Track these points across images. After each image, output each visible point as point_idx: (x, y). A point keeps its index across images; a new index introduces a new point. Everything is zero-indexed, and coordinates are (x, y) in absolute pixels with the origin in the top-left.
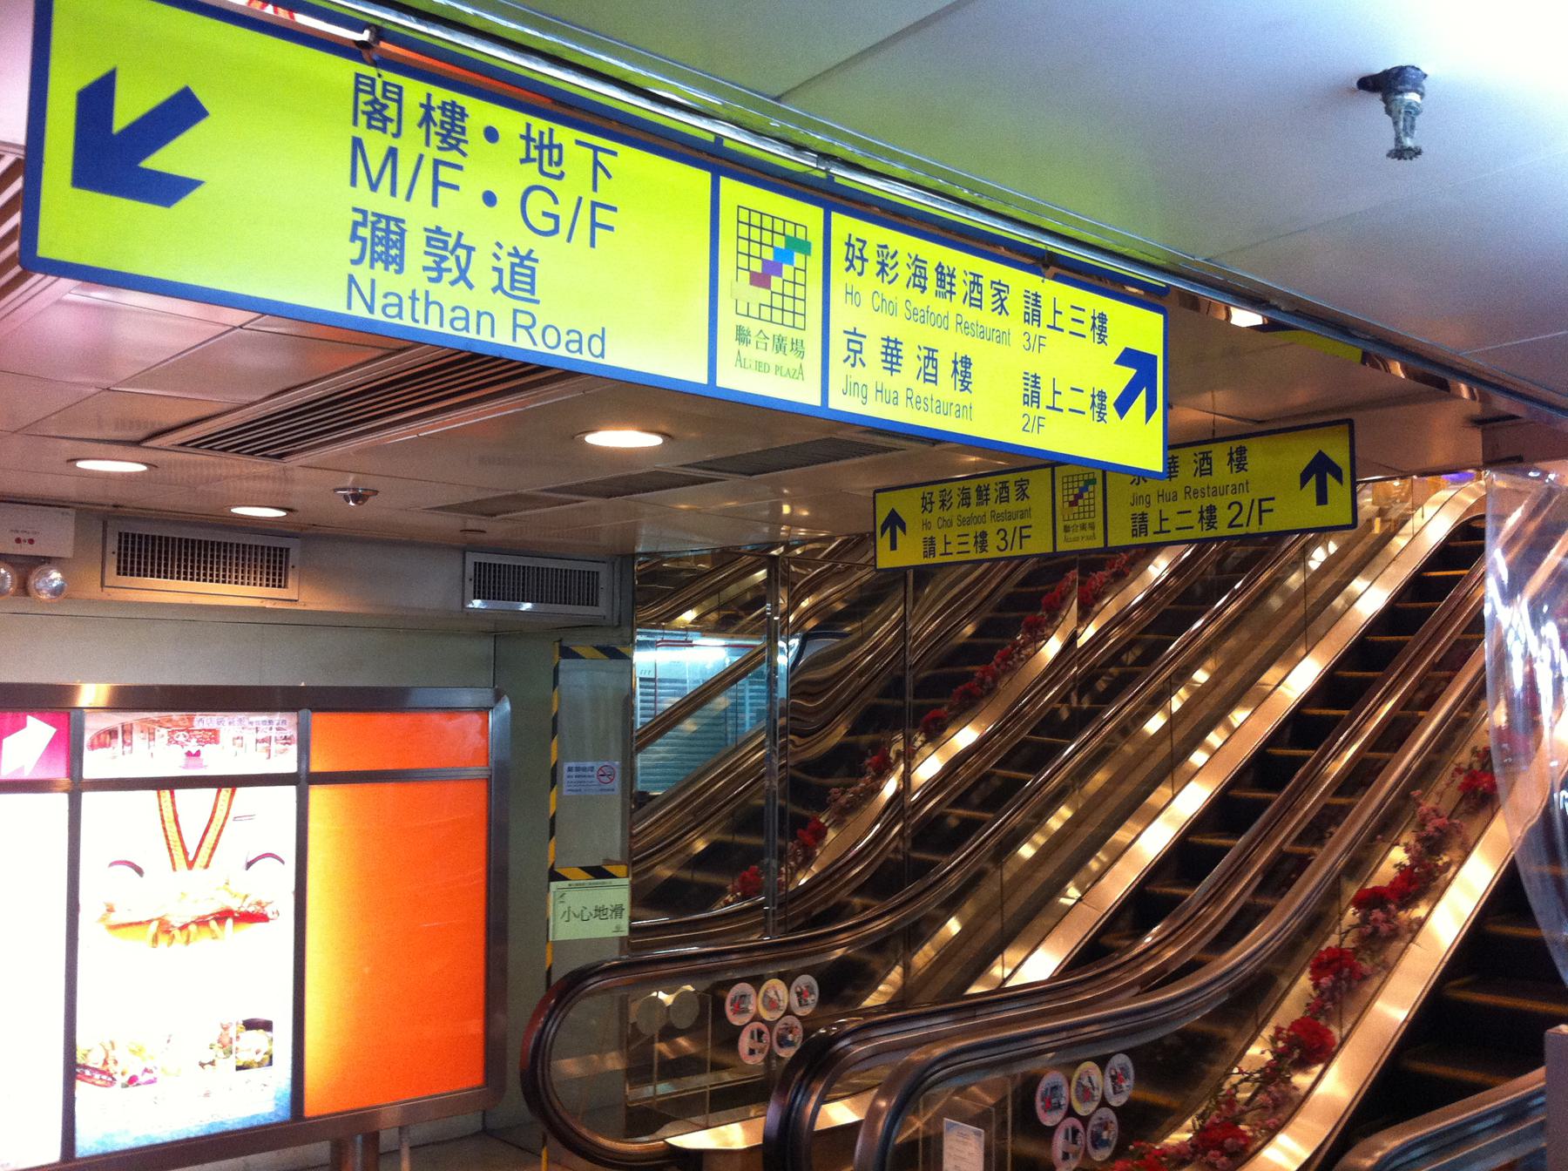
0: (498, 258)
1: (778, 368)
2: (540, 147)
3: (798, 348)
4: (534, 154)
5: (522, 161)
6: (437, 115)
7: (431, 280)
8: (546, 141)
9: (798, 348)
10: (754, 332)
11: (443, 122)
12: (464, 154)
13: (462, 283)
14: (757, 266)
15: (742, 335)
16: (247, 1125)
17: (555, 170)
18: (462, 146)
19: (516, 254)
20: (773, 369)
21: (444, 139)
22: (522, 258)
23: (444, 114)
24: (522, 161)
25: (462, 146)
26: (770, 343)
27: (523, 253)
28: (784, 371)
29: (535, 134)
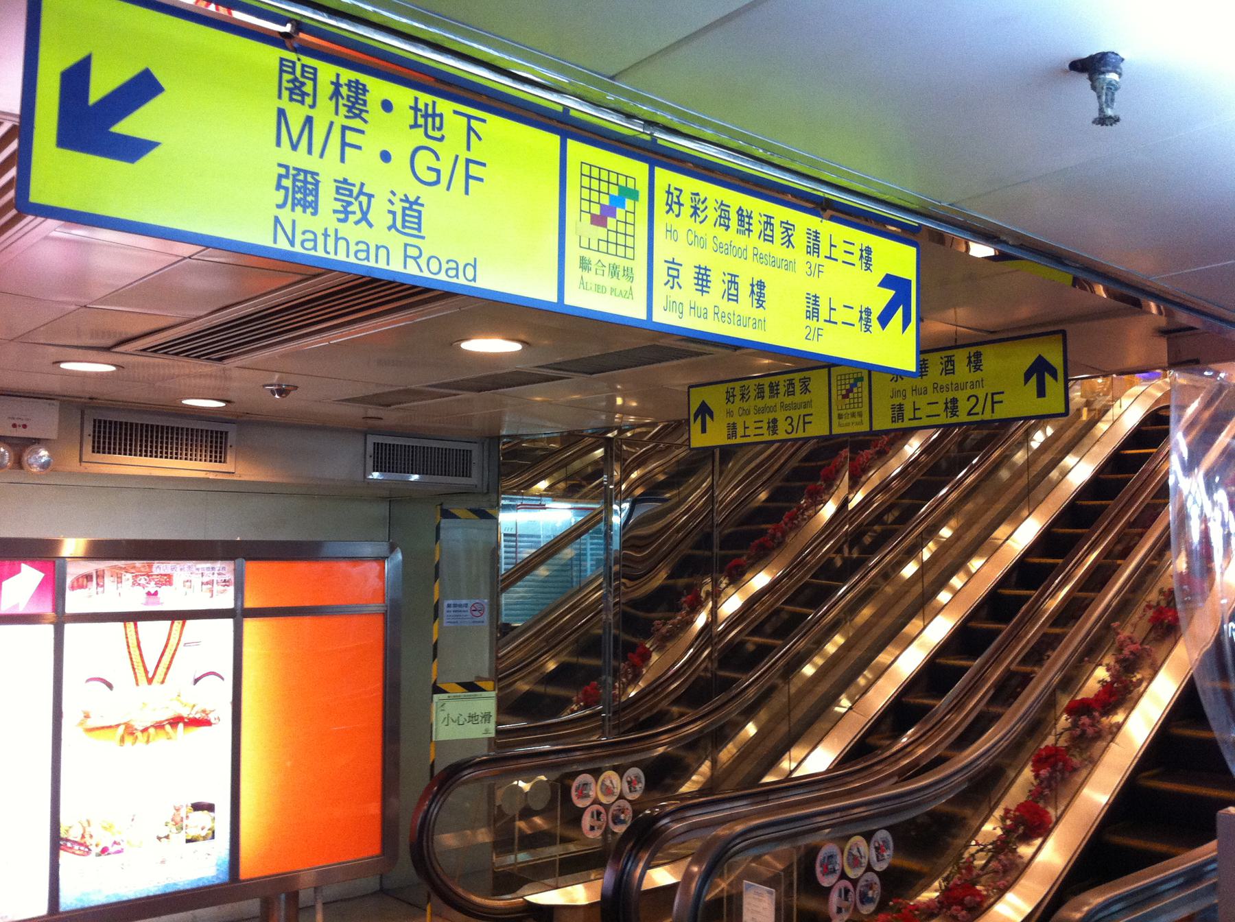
0: (392, 203)
1: (613, 290)
2: (426, 116)
3: (629, 274)
4: (421, 121)
5: (412, 127)
6: (344, 91)
7: (339, 220)
8: (430, 111)
9: (629, 274)
10: (594, 262)
11: (349, 96)
12: (365, 121)
13: (364, 223)
14: (596, 210)
15: (584, 264)
16: (194, 886)
17: (437, 134)
18: (364, 115)
19: (406, 200)
20: (609, 290)
21: (350, 109)
22: (411, 203)
23: (350, 90)
24: (412, 127)
25: (364, 115)
26: (607, 270)
27: (412, 199)
28: (618, 292)
29: (421, 106)
